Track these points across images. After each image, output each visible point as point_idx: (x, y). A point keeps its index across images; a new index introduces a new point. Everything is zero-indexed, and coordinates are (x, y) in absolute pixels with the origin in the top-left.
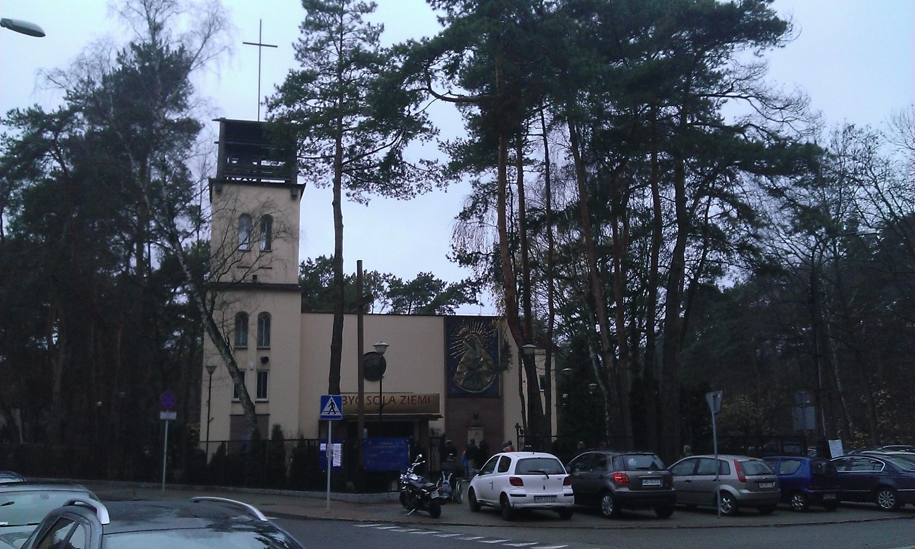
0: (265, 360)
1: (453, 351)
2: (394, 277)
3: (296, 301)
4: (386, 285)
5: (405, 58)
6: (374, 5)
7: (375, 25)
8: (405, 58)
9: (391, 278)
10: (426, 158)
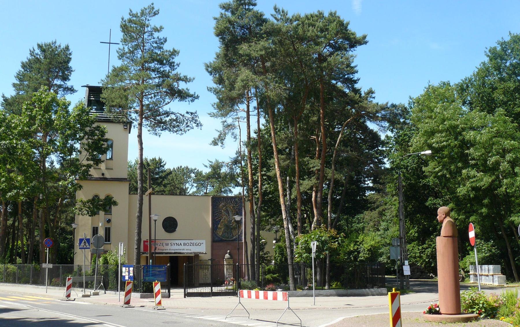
0: (109, 221)
1: (216, 216)
2: (198, 170)
3: (125, 187)
4: (193, 175)
5: (54, 106)
6: (161, 28)
7: (162, 38)
8: (54, 106)
9: (196, 171)
10: (190, 111)
